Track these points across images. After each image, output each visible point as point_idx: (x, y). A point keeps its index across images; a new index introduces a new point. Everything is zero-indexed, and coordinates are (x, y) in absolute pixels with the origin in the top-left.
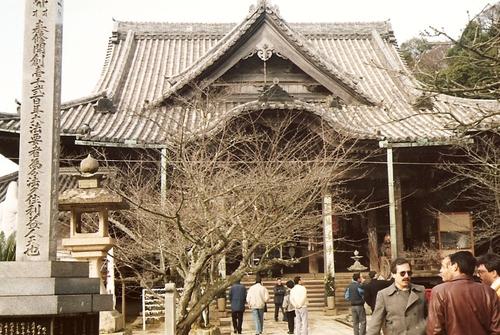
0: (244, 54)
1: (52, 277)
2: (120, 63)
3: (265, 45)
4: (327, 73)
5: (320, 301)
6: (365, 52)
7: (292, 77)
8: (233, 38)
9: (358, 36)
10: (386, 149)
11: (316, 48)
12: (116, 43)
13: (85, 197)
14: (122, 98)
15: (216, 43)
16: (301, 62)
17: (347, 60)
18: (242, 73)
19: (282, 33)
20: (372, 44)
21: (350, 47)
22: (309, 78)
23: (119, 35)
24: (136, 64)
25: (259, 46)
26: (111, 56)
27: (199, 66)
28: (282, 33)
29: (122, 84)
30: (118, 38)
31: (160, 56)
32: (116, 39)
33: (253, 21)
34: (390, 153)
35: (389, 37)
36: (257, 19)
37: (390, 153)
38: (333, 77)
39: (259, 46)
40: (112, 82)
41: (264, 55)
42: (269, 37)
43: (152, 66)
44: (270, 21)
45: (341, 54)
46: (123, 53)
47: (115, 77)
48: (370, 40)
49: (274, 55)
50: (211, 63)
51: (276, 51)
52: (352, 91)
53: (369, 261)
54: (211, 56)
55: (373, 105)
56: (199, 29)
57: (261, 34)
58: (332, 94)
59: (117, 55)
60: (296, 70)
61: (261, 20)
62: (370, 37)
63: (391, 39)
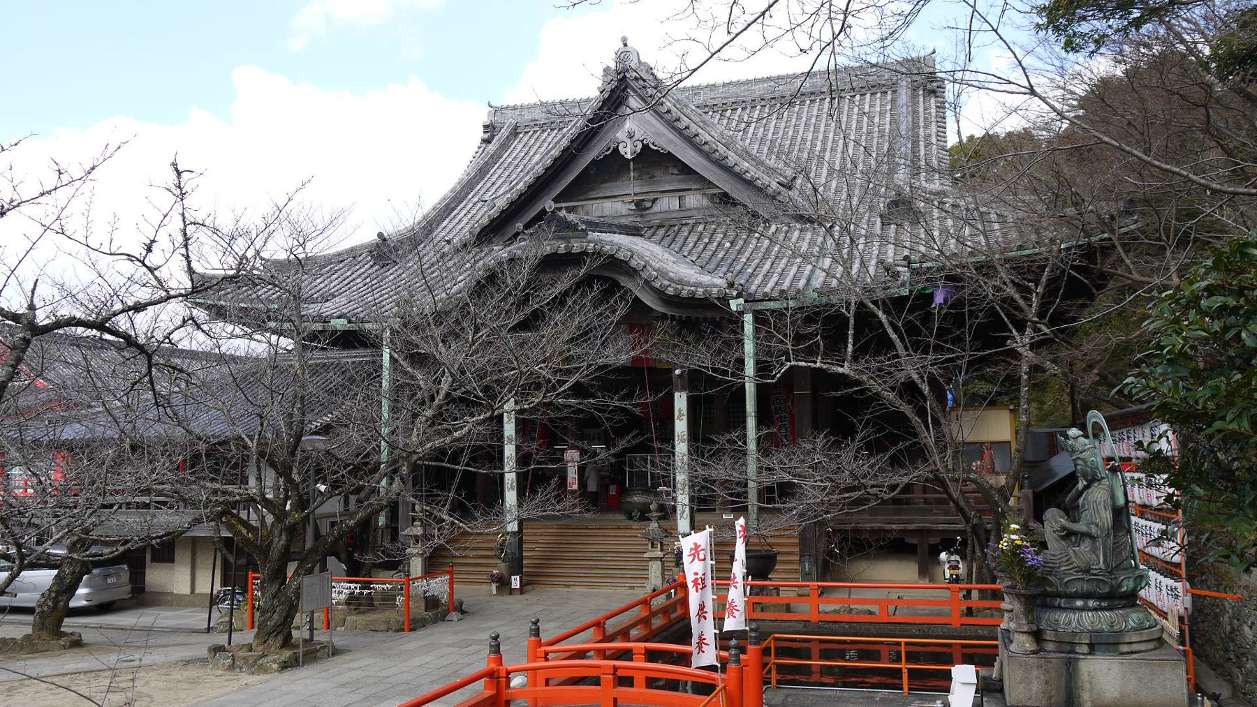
0: (596, 151)
1: (380, 235)
3: (634, 130)
5: (462, 565)
7: (679, 181)
10: (742, 313)
11: (714, 131)
18: (605, 182)
19: (654, 106)
22: (711, 185)
25: (621, 135)
34: (748, 318)
36: (612, 91)
37: (748, 318)
39: (621, 135)
41: (628, 150)
44: (635, 92)
49: (645, 147)
51: (649, 140)
53: (534, 492)
61: (624, 85)
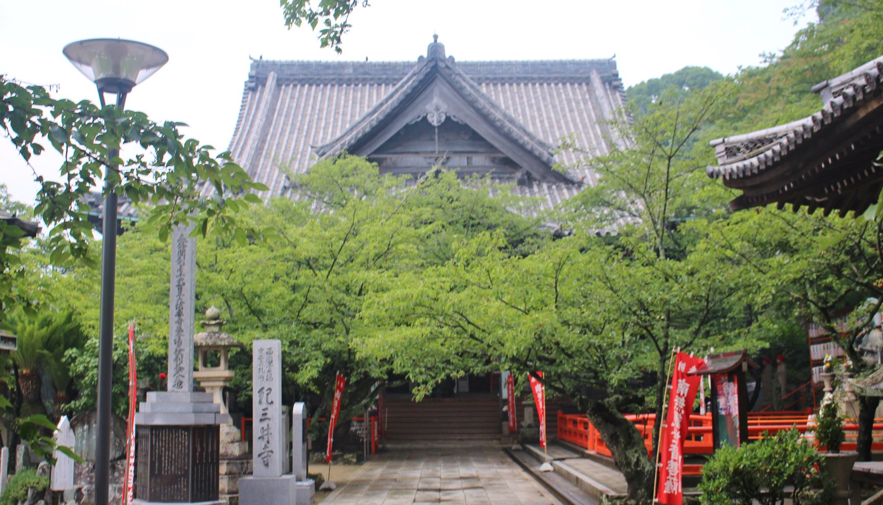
0: (409, 118)
2: (257, 121)
3: (435, 108)
4: (514, 142)
6: (577, 103)
8: (395, 97)
9: (572, 80)
12: (254, 90)
13: (734, 401)
14: (259, 171)
15: (391, 89)
16: (482, 129)
17: (552, 115)
20: (589, 91)
21: (559, 95)
22: (491, 148)
23: (258, 79)
24: (279, 121)
26: (247, 108)
27: (354, 133)
28: (458, 91)
29: (259, 150)
30: (256, 81)
31: (310, 108)
32: (253, 85)
33: (421, 77)
35: (612, 81)
36: (427, 74)
38: (522, 147)
39: (429, 107)
40: (248, 149)
42: (443, 96)
43: (298, 125)
45: (546, 106)
46: (262, 106)
47: (250, 142)
48: (587, 84)
49: (448, 119)
50: (368, 129)
51: (451, 114)
52: (546, 165)
54: (368, 120)
55: (573, 183)
56: (361, 70)
57: (432, 91)
58: (521, 167)
59: (254, 107)
60: (475, 137)
62: (588, 81)
63: (615, 83)
